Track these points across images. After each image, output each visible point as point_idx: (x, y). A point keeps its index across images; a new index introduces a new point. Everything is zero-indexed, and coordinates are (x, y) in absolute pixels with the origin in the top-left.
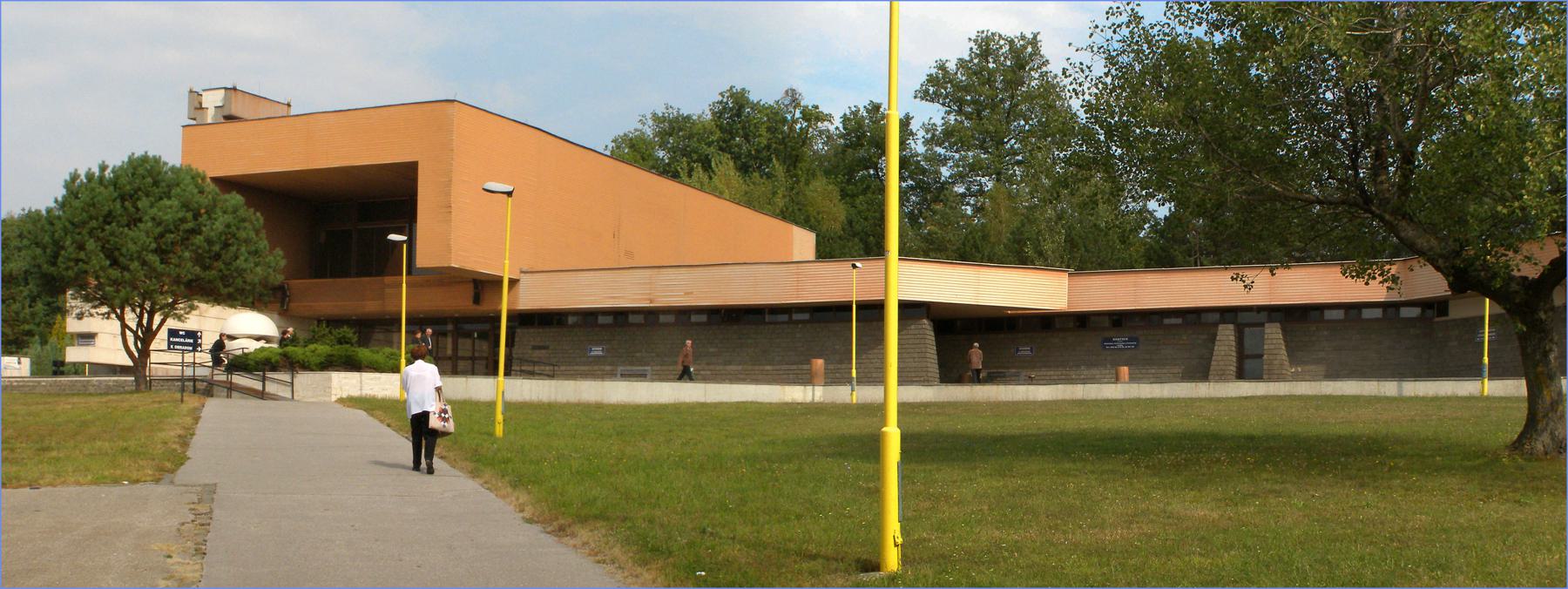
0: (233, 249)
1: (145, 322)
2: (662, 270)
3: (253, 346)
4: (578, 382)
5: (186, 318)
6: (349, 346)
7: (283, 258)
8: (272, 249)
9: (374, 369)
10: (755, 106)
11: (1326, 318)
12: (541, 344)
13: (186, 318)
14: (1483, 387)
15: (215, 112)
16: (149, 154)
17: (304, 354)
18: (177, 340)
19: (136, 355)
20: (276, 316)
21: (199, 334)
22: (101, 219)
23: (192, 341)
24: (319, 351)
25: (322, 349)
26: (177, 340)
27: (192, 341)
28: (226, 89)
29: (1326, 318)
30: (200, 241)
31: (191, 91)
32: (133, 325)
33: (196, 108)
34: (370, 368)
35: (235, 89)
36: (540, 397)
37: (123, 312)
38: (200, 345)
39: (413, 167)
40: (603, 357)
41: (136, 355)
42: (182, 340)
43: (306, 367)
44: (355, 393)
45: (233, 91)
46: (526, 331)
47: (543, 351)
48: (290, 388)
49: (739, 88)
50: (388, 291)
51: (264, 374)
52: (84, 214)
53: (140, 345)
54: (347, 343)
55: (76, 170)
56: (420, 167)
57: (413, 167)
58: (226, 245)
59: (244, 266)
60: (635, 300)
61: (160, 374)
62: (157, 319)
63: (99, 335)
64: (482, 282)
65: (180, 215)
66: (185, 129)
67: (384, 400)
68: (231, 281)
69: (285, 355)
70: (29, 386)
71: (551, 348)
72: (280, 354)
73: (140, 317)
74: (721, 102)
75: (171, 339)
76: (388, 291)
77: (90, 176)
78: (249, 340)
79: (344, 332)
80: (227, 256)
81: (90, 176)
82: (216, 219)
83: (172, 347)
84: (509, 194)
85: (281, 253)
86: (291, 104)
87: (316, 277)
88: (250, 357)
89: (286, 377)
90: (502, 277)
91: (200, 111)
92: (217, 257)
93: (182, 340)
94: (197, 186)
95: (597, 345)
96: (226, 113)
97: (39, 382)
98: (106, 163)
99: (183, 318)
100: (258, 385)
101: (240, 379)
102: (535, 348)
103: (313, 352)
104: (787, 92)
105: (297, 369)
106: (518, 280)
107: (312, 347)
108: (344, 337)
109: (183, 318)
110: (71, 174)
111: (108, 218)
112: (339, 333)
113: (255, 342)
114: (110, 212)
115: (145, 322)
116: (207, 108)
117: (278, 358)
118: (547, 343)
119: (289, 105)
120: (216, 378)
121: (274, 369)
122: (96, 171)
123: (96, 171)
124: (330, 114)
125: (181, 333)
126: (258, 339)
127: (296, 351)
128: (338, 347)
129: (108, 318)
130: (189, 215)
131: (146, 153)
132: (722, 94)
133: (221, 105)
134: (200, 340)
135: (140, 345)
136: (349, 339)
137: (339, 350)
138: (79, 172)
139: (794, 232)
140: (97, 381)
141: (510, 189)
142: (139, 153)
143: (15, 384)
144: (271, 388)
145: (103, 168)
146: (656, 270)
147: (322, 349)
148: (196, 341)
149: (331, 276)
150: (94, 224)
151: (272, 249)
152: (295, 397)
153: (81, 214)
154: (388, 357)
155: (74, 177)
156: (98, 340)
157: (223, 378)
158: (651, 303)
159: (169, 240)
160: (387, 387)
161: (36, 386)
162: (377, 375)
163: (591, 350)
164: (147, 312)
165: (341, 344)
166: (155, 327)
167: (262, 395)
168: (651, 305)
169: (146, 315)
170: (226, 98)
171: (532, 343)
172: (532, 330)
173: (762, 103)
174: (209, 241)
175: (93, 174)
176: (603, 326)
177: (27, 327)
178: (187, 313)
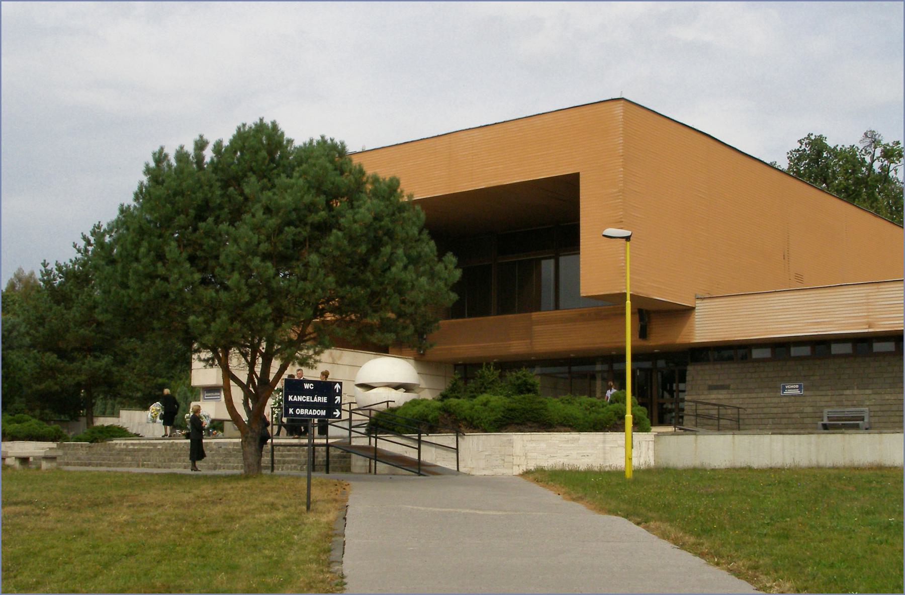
0: (387, 250)
1: (258, 369)
2: (882, 286)
3: (400, 398)
4: (847, 437)
5: (316, 361)
6: (531, 395)
7: (456, 267)
8: (441, 255)
9: (570, 426)
10: (833, 152)
11: (833, 353)
12: (719, 383)
13: (316, 361)
16: (265, 121)
17: (472, 408)
18: (300, 398)
19: (245, 417)
20: (412, 361)
21: (337, 386)
22: (192, 212)
23: (324, 400)
24: (492, 404)
25: (497, 400)
26: (300, 398)
27: (324, 400)
29: (833, 353)
30: (337, 238)
32: (243, 377)
34: (565, 426)
36: (797, 460)
37: (226, 355)
38: (339, 407)
39: (571, 183)
40: (799, 396)
41: (245, 417)
42: (308, 399)
43: (475, 425)
44: (547, 463)
46: (699, 368)
47: (723, 392)
48: (455, 455)
49: (816, 133)
50: (536, 328)
51: (420, 437)
52: (168, 205)
53: (251, 406)
54: (529, 391)
55: (162, 149)
56: (581, 176)
57: (571, 183)
58: (375, 249)
59: (404, 276)
60: (853, 324)
62: (276, 365)
64: (648, 312)
65: (308, 199)
67: (589, 473)
68: (383, 300)
69: (446, 410)
71: (732, 387)
72: (440, 409)
73: (252, 365)
74: (798, 151)
75: (290, 398)
76: (536, 328)
77: (181, 156)
78: (388, 388)
79: (524, 375)
80: (377, 263)
81: (181, 156)
82: (359, 207)
83: (291, 411)
84: (628, 238)
85: (454, 260)
88: (397, 413)
89: (448, 439)
90: (199, 401)
92: (364, 262)
93: (308, 399)
94: (332, 161)
95: (791, 380)
98: (205, 137)
99: (311, 361)
100: (412, 454)
101: (389, 445)
102: (711, 388)
103: (485, 404)
104: (866, 134)
105: (463, 429)
106: (693, 309)
107: (483, 397)
108: (525, 383)
109: (311, 361)
110: (154, 154)
111: (203, 210)
112: (518, 378)
113: (393, 391)
114: (206, 202)
115: (258, 369)
117: (436, 413)
118: (728, 382)
120: (355, 442)
121: (433, 429)
122: (190, 149)
123: (190, 149)
124: (475, 131)
125: (307, 386)
126: (397, 387)
127: (462, 404)
128: (517, 397)
129: (211, 365)
130: (321, 200)
131: (261, 120)
132: (800, 142)
134: (338, 398)
135: (251, 406)
136: (533, 385)
137: (519, 401)
138: (166, 151)
140: (216, 443)
141: (627, 233)
142: (251, 121)
143: (131, 447)
144: (429, 456)
145: (201, 145)
146: (875, 287)
147: (497, 400)
148: (331, 399)
149: (470, 316)
150: (181, 219)
151: (441, 255)
152: (460, 470)
153: (164, 206)
154: (587, 409)
155: (160, 157)
157: (364, 442)
158: (869, 328)
159: (290, 237)
160: (590, 451)
161: (150, 450)
162: (575, 435)
163: (784, 389)
164: (262, 355)
165: (521, 392)
166: (271, 377)
167: (418, 468)
168: (871, 330)
169: (260, 360)
171: (710, 383)
172: (707, 367)
173: (838, 148)
174: (352, 239)
175: (187, 155)
176: (758, 360)
177: (160, 381)
178: (317, 353)
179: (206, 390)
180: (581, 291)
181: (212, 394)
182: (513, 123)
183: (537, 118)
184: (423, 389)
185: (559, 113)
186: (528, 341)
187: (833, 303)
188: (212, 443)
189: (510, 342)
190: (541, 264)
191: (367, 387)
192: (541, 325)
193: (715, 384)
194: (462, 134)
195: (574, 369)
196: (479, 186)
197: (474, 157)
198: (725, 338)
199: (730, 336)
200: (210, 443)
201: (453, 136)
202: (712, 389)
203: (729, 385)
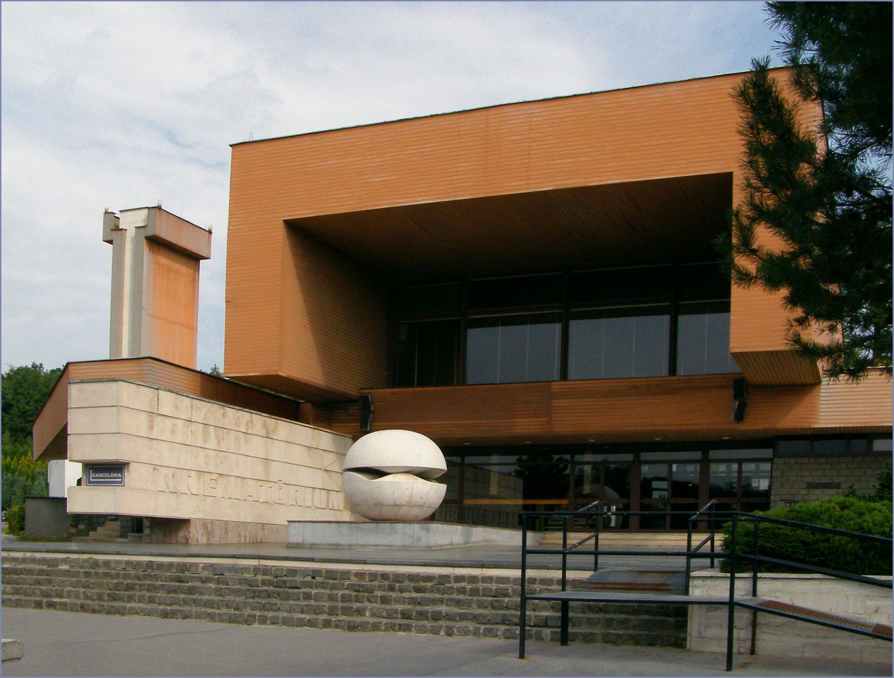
12: (824, 480)
14: (703, 521)
15: (136, 232)
28: (148, 208)
31: (106, 213)
33: (112, 230)
35: (159, 208)
45: (157, 211)
50: (558, 403)
61: (232, 538)
63: (132, 466)
66: (236, 149)
70: (29, 572)
86: (212, 231)
87: (393, 387)
91: (119, 233)
96: (150, 233)
97: (54, 563)
116: (126, 230)
118: (837, 480)
119: (210, 232)
133: (142, 225)
139: (67, 467)
156: (132, 476)
170: (149, 216)
171: (809, 480)
179: (93, 469)
180: (731, 345)
181: (106, 475)
182: (606, 96)
183: (654, 90)
184: (512, 476)
185: (696, 85)
186: (546, 419)
187: (866, 393)
188: (196, 564)
189: (512, 420)
190: (465, 336)
191: (376, 473)
192: (563, 399)
193: (817, 480)
194: (510, 109)
195: (469, 460)
196: (542, 187)
197: (533, 144)
198: (866, 423)
199: (876, 420)
200: (191, 564)
201: (492, 112)
202: (813, 488)
203: (840, 483)
